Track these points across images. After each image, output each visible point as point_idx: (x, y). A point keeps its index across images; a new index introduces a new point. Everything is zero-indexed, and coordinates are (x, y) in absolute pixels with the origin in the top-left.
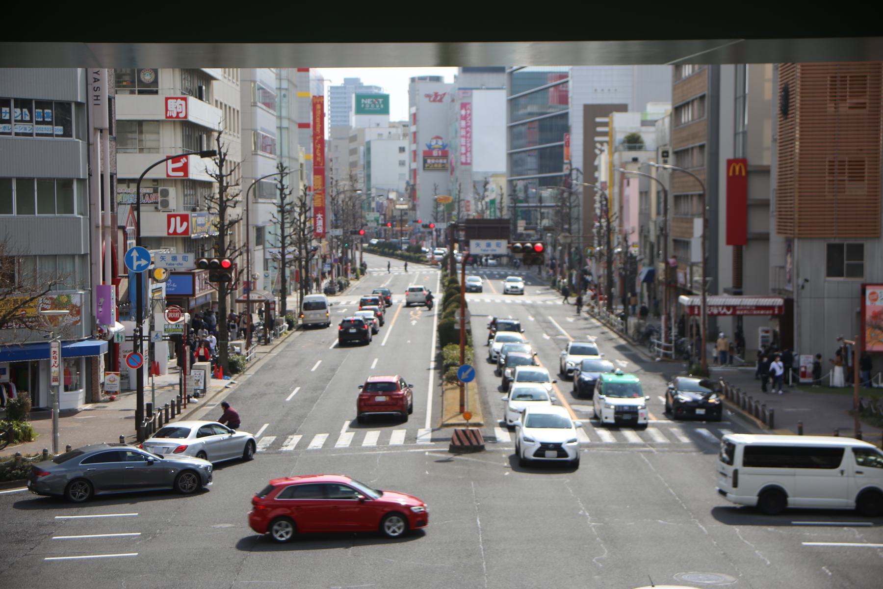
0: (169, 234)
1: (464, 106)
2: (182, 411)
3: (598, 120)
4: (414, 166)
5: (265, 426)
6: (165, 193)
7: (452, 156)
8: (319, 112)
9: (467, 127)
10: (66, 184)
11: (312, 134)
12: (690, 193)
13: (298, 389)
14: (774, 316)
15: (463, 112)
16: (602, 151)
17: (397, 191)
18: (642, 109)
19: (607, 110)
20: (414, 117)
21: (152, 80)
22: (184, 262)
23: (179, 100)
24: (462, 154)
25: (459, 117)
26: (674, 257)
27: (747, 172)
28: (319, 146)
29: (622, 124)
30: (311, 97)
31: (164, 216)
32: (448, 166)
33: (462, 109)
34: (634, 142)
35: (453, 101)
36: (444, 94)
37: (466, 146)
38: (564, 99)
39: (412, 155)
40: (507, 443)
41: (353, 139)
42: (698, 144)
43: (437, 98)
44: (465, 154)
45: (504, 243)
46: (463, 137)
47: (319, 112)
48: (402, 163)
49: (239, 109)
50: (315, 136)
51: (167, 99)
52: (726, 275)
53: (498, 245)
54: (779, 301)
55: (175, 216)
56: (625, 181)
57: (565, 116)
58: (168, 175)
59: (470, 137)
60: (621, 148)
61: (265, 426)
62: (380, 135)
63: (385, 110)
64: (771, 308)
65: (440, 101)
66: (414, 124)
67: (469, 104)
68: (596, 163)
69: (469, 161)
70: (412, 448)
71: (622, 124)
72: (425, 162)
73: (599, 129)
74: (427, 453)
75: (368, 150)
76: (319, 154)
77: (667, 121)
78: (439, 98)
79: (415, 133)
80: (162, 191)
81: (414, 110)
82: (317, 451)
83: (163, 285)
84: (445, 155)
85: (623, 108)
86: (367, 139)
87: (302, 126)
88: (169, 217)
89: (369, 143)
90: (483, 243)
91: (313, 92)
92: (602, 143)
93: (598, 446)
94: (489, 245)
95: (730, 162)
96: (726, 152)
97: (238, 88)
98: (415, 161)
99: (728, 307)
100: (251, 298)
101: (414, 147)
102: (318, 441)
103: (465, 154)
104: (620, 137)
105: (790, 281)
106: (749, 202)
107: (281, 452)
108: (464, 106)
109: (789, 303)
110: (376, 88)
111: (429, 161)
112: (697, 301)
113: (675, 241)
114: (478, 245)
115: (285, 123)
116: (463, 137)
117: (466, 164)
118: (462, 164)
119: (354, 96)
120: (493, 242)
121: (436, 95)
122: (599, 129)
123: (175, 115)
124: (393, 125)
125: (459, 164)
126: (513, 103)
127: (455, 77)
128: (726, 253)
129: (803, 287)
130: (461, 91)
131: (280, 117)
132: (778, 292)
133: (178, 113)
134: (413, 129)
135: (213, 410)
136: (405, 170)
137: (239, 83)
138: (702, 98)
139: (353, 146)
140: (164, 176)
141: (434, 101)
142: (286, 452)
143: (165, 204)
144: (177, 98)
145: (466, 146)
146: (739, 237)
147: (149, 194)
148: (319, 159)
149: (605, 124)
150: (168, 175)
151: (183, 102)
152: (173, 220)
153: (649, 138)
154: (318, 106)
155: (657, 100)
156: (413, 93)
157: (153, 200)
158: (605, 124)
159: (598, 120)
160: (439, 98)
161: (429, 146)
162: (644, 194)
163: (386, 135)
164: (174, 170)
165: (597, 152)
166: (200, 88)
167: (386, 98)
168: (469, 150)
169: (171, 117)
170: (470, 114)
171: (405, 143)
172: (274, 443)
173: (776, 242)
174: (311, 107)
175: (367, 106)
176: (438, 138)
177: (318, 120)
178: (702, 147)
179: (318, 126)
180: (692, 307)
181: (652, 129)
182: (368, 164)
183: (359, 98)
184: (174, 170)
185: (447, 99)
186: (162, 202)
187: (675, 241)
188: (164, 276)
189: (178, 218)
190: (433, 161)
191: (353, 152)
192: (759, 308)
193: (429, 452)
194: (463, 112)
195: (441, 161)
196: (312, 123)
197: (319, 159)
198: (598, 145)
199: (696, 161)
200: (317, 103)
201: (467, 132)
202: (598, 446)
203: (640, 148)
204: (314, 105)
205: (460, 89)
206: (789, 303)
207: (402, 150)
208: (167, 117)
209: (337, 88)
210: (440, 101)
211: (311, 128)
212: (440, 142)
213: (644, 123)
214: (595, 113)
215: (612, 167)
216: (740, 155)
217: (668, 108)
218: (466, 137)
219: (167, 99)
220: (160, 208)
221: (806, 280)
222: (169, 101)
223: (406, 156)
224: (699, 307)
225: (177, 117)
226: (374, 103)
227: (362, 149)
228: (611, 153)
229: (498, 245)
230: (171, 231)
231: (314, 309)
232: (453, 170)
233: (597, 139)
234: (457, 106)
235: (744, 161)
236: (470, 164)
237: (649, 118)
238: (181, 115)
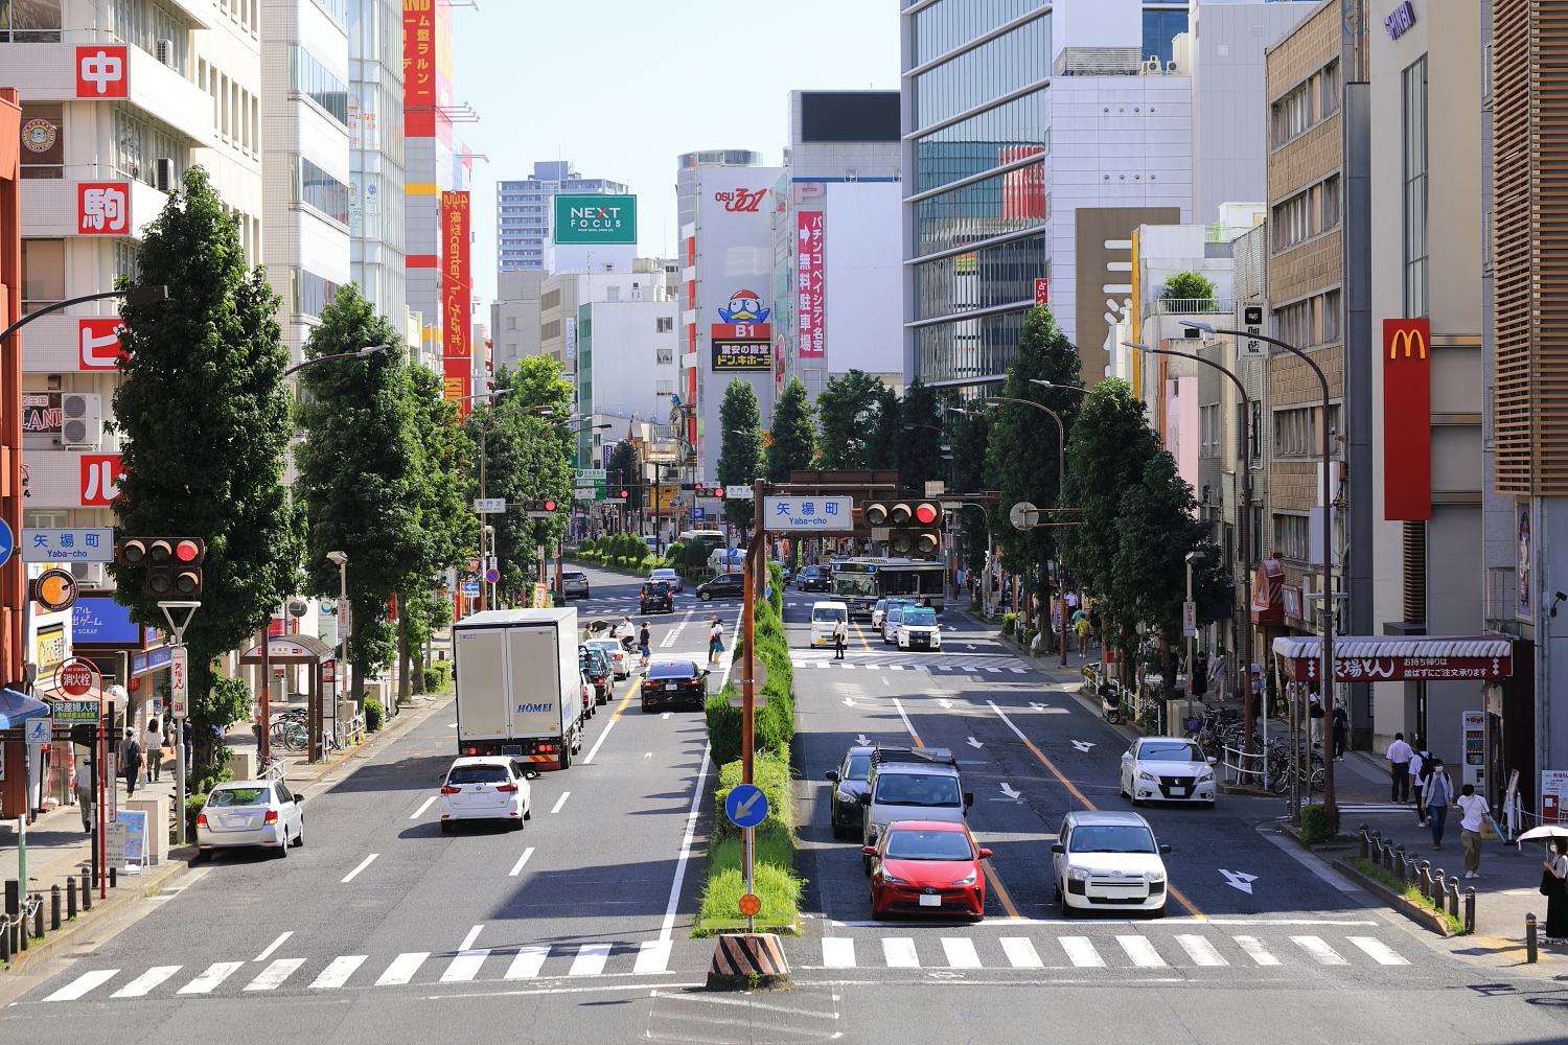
0: (85, 501)
1: (806, 219)
2: (94, 903)
3: (1110, 244)
4: (691, 360)
5: (286, 936)
6: (77, 407)
7: (777, 337)
8: (456, 230)
9: (814, 267)
11: (440, 279)
12: (1309, 405)
13: (372, 857)
14: (1491, 680)
15: (805, 234)
16: (1119, 318)
17: (652, 422)
18: (1211, 219)
19: (1125, 221)
20: (691, 248)
21: (48, 146)
22: (89, 549)
23: (110, 190)
24: (802, 331)
25: (794, 245)
26: (1278, 556)
27: (1430, 350)
28: (457, 310)
29: (1164, 253)
30: (439, 196)
31: (73, 460)
32: (772, 360)
33: (801, 227)
34: (1186, 294)
35: (781, 208)
36: (762, 192)
37: (811, 312)
38: (1037, 204)
39: (687, 333)
40: (848, 970)
41: (551, 300)
42: (1323, 291)
43: (744, 201)
44: (811, 332)
45: (845, 504)
46: (803, 291)
47: (456, 230)
48: (664, 358)
49: (259, 217)
50: (447, 284)
51: (82, 188)
52: (1389, 600)
53: (830, 509)
54: (1503, 648)
55: (99, 460)
56: (1170, 384)
57: (1037, 242)
58: (83, 366)
59: (821, 293)
60: (1160, 307)
61: (286, 936)
62: (613, 291)
63: (627, 234)
64: (1484, 661)
65: (752, 208)
66: (692, 263)
67: (820, 214)
68: (1107, 346)
69: (818, 349)
70: (620, 981)
71: (1164, 253)
72: (716, 351)
73: (1113, 266)
74: (654, 994)
75: (585, 327)
76: (457, 329)
77: (1257, 238)
78: (749, 200)
79: (693, 283)
80: (70, 401)
81: (689, 230)
82: (396, 988)
83: (66, 617)
84: (763, 337)
85: (1170, 216)
86: (583, 301)
87: (413, 261)
88: (87, 461)
89: (587, 308)
90: (796, 504)
91: (444, 182)
92: (1120, 299)
93: (1059, 975)
94: (809, 509)
95: (1390, 326)
96: (1386, 304)
97: (258, 168)
98: (692, 349)
99: (1385, 662)
100: (271, 653)
101: (690, 317)
102: (403, 968)
103: (811, 332)
105: (1526, 599)
106: (1434, 420)
107: (312, 992)
109: (1524, 649)
110: (611, 184)
111: (726, 349)
112: (1313, 647)
113: (1277, 517)
114: (783, 508)
115: (377, 254)
116: (803, 291)
117: (812, 354)
118: (803, 353)
119: (552, 198)
120: (819, 502)
121: (742, 193)
122: (1113, 266)
123: (99, 225)
124: (641, 267)
125: (795, 354)
126: (920, 216)
127: (786, 153)
128: (1389, 538)
129: (1554, 612)
130: (800, 185)
131: (360, 241)
132: (1506, 627)
133: (107, 221)
134: (689, 274)
135: (169, 903)
136: (671, 372)
137: (259, 156)
138: (1331, 181)
139: (548, 316)
140: (75, 367)
141: (737, 208)
142: (324, 991)
143: (78, 432)
144: (104, 186)
145: (811, 312)
146: (1416, 504)
147: (40, 409)
148: (456, 339)
149: (1124, 255)
150: (83, 366)
151: (120, 196)
152: (94, 468)
153: (1222, 280)
154: (456, 217)
155: (1241, 196)
156: (687, 190)
157: (48, 422)
158: (1124, 255)
159: (1110, 244)
160: (749, 200)
161: (726, 315)
162: (1210, 409)
163: (626, 291)
164: (97, 352)
165: (1109, 317)
166: (163, 165)
167: (628, 204)
168: (818, 322)
169: (92, 230)
170: (821, 239)
171: (670, 307)
172: (298, 972)
173: (1499, 505)
174: (439, 219)
175: (584, 224)
176: (747, 294)
177: (455, 247)
178: (1332, 295)
179: (456, 261)
180: (1301, 662)
181: (1227, 263)
182: (585, 360)
183: (564, 205)
184: (97, 352)
185: (766, 205)
186: (69, 425)
187: (1277, 517)
188: (64, 596)
189: (107, 465)
190: (736, 350)
191: (551, 330)
192: (1455, 662)
193: (659, 990)
194: (805, 234)
195: (754, 349)
196: (440, 254)
197: (456, 339)
198: (1111, 304)
199: (1321, 332)
200: (455, 211)
201: (814, 281)
202: (1059, 975)
203: (1204, 307)
204: (446, 213)
205: (795, 180)
206: (1524, 649)
207: (664, 324)
208: (81, 230)
209: (520, 184)
210: (752, 208)
211: (439, 270)
212: (752, 306)
213: (1213, 250)
214: (1104, 228)
215: (1138, 349)
216: (1417, 312)
217: (1261, 210)
218: (812, 292)
219: (82, 188)
220: (64, 441)
221: (1561, 596)
222: (88, 192)
223: (672, 340)
224: (1316, 660)
225: (106, 229)
226: (598, 215)
227: (570, 324)
228: (1139, 322)
229: (830, 509)
230: (90, 494)
231: (510, 741)
232: (781, 369)
233: (1109, 289)
234: (790, 220)
235: (1423, 324)
236: (821, 354)
237: (1224, 237)
238: (114, 225)
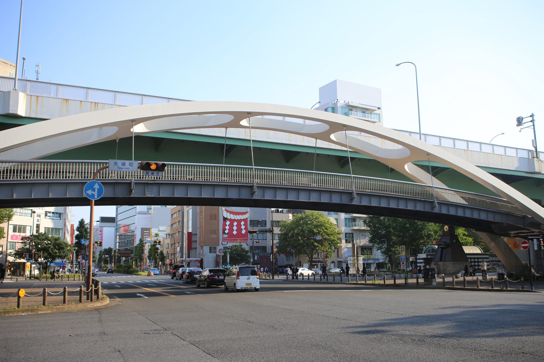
1: (101, 231)
10: (59, 229)
104: (153, 234)
108: (101, 231)
109: (202, 260)
